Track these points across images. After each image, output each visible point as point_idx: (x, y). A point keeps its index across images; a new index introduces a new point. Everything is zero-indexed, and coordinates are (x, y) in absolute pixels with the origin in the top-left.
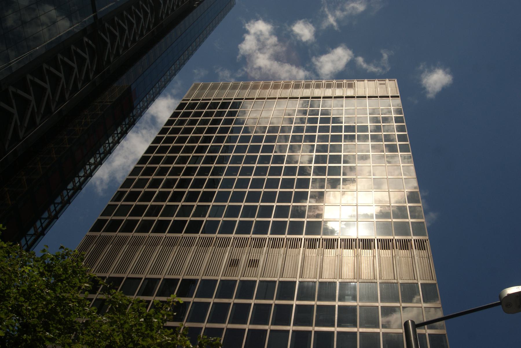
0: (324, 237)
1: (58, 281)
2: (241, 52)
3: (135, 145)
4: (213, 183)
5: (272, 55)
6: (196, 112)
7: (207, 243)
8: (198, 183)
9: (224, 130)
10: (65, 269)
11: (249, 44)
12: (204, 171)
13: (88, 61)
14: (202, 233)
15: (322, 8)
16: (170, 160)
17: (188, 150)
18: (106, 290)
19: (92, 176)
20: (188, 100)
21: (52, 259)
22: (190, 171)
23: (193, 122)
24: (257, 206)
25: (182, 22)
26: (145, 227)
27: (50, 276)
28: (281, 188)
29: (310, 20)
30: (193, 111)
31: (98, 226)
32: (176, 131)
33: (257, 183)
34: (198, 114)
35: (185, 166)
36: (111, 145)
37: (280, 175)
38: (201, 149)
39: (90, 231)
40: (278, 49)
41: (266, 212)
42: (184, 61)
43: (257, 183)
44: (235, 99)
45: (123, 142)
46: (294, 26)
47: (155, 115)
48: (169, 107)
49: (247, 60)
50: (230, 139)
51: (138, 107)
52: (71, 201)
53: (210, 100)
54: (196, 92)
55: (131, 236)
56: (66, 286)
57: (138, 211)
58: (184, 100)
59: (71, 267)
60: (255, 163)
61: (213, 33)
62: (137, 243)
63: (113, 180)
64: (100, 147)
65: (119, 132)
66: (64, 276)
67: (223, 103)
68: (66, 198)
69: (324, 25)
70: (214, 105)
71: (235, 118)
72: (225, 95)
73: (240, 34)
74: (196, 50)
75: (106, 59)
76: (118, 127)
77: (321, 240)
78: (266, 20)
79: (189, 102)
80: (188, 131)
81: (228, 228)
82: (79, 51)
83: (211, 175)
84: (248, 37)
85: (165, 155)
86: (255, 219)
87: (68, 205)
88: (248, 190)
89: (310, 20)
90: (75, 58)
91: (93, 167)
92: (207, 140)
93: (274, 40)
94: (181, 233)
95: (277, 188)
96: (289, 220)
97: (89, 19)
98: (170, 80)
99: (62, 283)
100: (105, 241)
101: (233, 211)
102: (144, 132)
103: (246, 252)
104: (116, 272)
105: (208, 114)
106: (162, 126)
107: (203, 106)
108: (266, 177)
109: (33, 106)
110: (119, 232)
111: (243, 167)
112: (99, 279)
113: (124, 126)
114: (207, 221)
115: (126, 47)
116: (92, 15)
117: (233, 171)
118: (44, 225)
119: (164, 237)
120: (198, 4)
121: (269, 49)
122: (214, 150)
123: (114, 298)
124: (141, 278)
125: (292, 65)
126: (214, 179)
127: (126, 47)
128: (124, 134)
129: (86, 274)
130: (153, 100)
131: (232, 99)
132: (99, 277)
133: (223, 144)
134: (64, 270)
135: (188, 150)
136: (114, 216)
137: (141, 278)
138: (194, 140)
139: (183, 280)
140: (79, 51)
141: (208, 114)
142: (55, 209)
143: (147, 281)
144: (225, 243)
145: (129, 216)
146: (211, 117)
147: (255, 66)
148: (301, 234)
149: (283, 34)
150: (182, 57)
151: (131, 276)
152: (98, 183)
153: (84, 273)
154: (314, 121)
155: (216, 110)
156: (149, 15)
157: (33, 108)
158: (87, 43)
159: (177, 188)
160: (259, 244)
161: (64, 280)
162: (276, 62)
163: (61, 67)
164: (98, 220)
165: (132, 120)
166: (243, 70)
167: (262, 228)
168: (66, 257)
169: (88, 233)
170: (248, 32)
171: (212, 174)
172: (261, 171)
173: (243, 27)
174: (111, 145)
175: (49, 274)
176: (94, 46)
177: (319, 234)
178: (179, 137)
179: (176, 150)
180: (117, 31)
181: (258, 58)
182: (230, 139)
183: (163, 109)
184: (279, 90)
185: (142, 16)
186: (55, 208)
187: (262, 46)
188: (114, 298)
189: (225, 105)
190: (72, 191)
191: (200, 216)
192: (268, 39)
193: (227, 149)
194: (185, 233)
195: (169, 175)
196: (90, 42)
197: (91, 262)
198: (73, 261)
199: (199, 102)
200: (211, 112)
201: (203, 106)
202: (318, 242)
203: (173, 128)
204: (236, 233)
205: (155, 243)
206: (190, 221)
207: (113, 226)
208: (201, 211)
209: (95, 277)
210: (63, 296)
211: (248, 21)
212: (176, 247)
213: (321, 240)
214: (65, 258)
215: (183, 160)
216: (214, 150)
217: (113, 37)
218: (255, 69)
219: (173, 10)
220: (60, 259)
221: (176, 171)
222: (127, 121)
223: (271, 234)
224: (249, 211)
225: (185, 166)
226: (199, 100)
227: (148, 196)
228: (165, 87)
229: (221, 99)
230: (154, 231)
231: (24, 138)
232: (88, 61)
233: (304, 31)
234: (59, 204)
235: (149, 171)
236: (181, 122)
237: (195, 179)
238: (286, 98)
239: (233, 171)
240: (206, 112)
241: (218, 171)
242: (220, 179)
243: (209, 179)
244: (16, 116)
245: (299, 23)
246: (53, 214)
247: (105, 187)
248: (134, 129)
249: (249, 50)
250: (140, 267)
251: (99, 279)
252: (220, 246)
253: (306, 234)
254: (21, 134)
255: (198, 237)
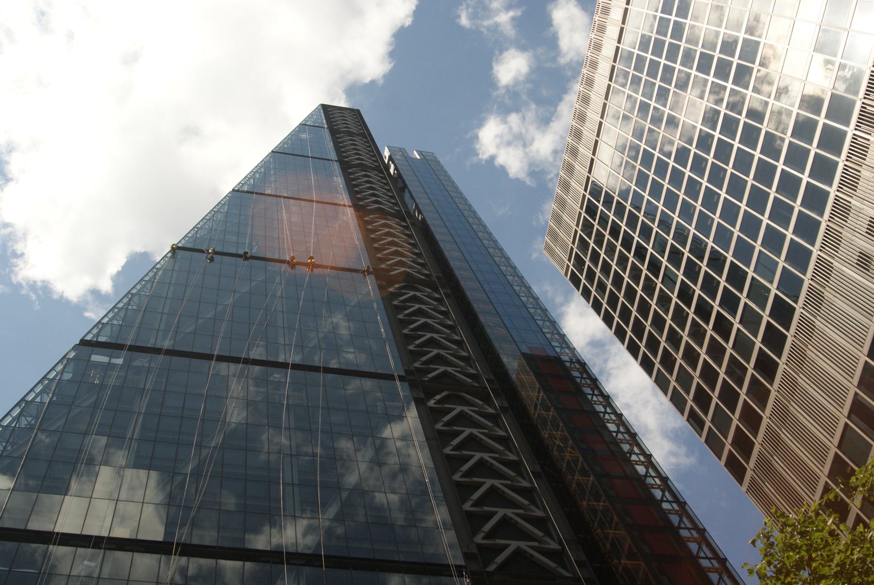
0: (862, 94)
1: (809, 566)
2: (522, 175)
3: (631, 389)
4: (717, 261)
5: (538, 128)
6: (591, 260)
7: (816, 299)
8: (710, 286)
9: (632, 221)
10: (793, 547)
11: (513, 161)
12: (692, 271)
13: (466, 409)
14: (796, 302)
15: (482, 30)
16: (659, 322)
17: (649, 288)
18: (850, 491)
19: (667, 478)
20: (568, 266)
21: (769, 563)
22: (686, 295)
23: (606, 268)
24: (775, 198)
25: (442, 245)
26: (760, 394)
27: (795, 575)
28: (755, 150)
29: (497, 52)
30: (587, 263)
31: (736, 469)
32: (613, 301)
33: (736, 187)
34: (595, 257)
35: (675, 299)
36: (608, 410)
37: (732, 145)
38: (654, 266)
39: (741, 485)
40: (530, 116)
41: (789, 185)
42: (487, 232)
43: (736, 187)
44: (586, 190)
45: (619, 403)
46: (499, 81)
47: (588, 340)
48: (582, 315)
49: (537, 170)
50: (648, 214)
51: (558, 350)
52: (682, 500)
53: (576, 231)
54: (558, 250)
55: (768, 420)
56: (821, 555)
57: (729, 396)
58: (566, 274)
59: (791, 537)
60: (701, 184)
61: (481, 214)
62: (782, 413)
63: (675, 436)
64: (607, 428)
65: (603, 410)
66: (803, 553)
67: (586, 212)
68: (675, 506)
69: (510, 31)
70: (587, 227)
71: (616, 198)
72: (575, 206)
73: (493, 171)
74: (490, 234)
75: (469, 380)
76: (571, 375)
77: (866, 101)
78: (481, 124)
79: (571, 267)
80: (618, 281)
81: (799, 257)
82: (446, 418)
83: (702, 262)
84: (501, 160)
85: (648, 328)
86: (797, 206)
87: (687, 507)
88: (743, 206)
89: (497, 52)
90: (455, 428)
91: (636, 450)
92: (641, 253)
93: (514, 119)
94: (786, 336)
95: (753, 156)
96: (813, 149)
97: (402, 389)
98: (536, 299)
99: (814, 560)
100: (764, 465)
101: (774, 240)
102: (611, 364)
103: (850, 236)
104: (823, 464)
105: (599, 241)
106: (610, 333)
107: (584, 245)
108: (730, 169)
109: (514, 513)
110: (755, 438)
111: (702, 205)
112: (825, 498)
113: (583, 381)
114: (778, 289)
115: (459, 343)
116: (398, 383)
117: (704, 224)
118: (710, 555)
119: (785, 366)
120: (420, 212)
121: (527, 130)
122: (660, 245)
123: (863, 485)
124: (846, 424)
125: (561, 99)
126: (709, 259)
127: (459, 343)
128: (607, 399)
129: (810, 517)
130: (563, 337)
131: (584, 196)
132: (822, 497)
133: (655, 229)
134: (793, 550)
135: (649, 288)
136: (726, 438)
137: (846, 424)
138: (636, 274)
139: (869, 356)
140: (446, 418)
141: (599, 241)
142: (689, 529)
143: (853, 416)
144: (825, 269)
145: (733, 414)
146: (604, 236)
147: (551, 159)
148: (845, 133)
149: (510, 102)
150: (496, 259)
151: (836, 440)
152: (673, 460)
153: (807, 520)
154: (654, 65)
155: (596, 226)
156: (418, 294)
157: (517, 514)
158: (438, 402)
159: (707, 323)
160: (842, 210)
161: (810, 556)
162: (551, 124)
163: (464, 452)
164: (726, 465)
165: (577, 365)
166: (551, 180)
167: (815, 199)
168: (772, 540)
169: (744, 488)
170: (493, 158)
171: (701, 259)
172: (717, 176)
173: (483, 162)
174: (622, 429)
175: (792, 576)
176: (444, 394)
177: (854, 103)
178: (645, 347)
179: (644, 308)
180: (431, 352)
181: (538, 151)
182: (648, 214)
183: (581, 326)
184: (588, 114)
185: (417, 306)
186: (686, 528)
187: (520, 140)
188: (863, 485)
189: (591, 210)
190: (667, 494)
191: (767, 299)
192: (511, 128)
193: (665, 224)
194: (788, 330)
195: (683, 330)
196: (438, 397)
197: (796, 501)
198: (782, 531)
199: (575, 250)
200: (596, 235)
201: (584, 245)
202: (868, 108)
203: (608, 303)
204: (813, 245)
205: (791, 384)
206: (770, 316)
207: (744, 445)
208: (758, 293)
209: (820, 504)
210: (837, 565)
211: (474, 152)
212: (808, 351)
213: (866, 101)
214: (773, 543)
215: (664, 301)
216: (660, 245)
217: (439, 359)
218: (555, 160)
219: (419, 255)
220: (772, 551)
221: (680, 317)
222: (576, 374)
223: (830, 185)
224: (781, 213)
225: (675, 299)
226: (572, 249)
227: (709, 375)
228: (545, 311)
229: (580, 214)
230: (771, 380)
231: (561, 543)
232: (466, 409)
233: (512, 68)
234: (681, 521)
235: (668, 361)
236: (602, 287)
237: (701, 290)
238: (605, 105)
239: (704, 224)
240: (594, 243)
241: (698, 248)
242: (712, 247)
243: (707, 266)
244: (523, 545)
245: (498, 71)
246: (695, 535)
247: (683, 450)
248: (602, 380)
249: (522, 162)
250: (835, 392)
251: (825, 498)
252: (827, 278)
253: (847, 124)
254: (554, 545)
255: (802, 310)
